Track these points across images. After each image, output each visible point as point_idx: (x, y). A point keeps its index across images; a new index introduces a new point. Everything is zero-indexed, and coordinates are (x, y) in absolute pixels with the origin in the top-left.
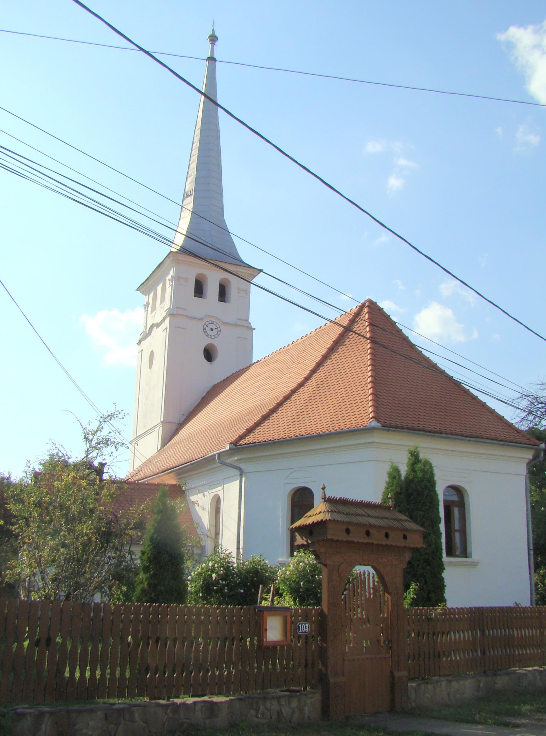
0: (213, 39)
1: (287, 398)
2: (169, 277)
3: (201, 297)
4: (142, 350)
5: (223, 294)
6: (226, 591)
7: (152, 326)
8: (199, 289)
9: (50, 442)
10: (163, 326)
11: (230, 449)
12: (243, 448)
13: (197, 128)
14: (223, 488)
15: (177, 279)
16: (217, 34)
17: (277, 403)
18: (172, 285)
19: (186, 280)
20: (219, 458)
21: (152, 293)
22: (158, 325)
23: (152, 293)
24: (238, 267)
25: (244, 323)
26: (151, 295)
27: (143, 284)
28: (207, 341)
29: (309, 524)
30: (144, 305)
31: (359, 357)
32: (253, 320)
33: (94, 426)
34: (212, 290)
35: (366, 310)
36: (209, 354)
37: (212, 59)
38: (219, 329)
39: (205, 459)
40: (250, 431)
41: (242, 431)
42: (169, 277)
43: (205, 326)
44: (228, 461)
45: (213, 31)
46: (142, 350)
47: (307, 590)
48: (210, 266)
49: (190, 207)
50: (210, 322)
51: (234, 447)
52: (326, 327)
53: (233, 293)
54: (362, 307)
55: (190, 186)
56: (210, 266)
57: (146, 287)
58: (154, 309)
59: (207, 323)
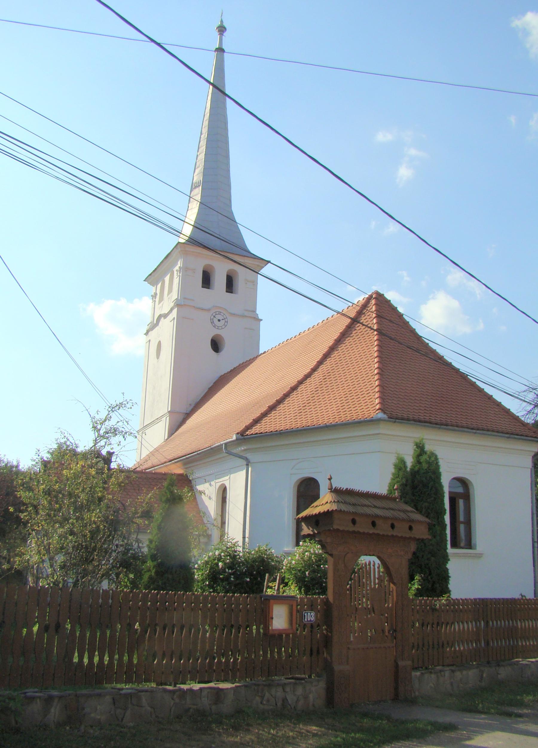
0: (222, 29)
2: (177, 268)
4: (150, 341)
6: (232, 579)
8: (207, 280)
9: (59, 431)
10: (171, 317)
11: (237, 439)
13: (205, 119)
14: (230, 478)
15: (185, 270)
16: (225, 25)
20: (226, 448)
21: (160, 284)
22: (165, 316)
23: (160, 284)
24: (246, 258)
26: (159, 286)
27: (150, 275)
28: (216, 332)
30: (152, 296)
31: (366, 349)
32: (260, 312)
33: (103, 415)
36: (216, 345)
37: (220, 50)
38: (226, 320)
39: (211, 449)
40: (256, 421)
41: (249, 421)
42: (177, 268)
45: (222, 21)
46: (150, 341)
47: (312, 579)
48: (217, 259)
49: (198, 198)
50: (218, 313)
53: (240, 284)
55: (198, 177)
56: (217, 259)
57: (154, 277)
58: (161, 299)
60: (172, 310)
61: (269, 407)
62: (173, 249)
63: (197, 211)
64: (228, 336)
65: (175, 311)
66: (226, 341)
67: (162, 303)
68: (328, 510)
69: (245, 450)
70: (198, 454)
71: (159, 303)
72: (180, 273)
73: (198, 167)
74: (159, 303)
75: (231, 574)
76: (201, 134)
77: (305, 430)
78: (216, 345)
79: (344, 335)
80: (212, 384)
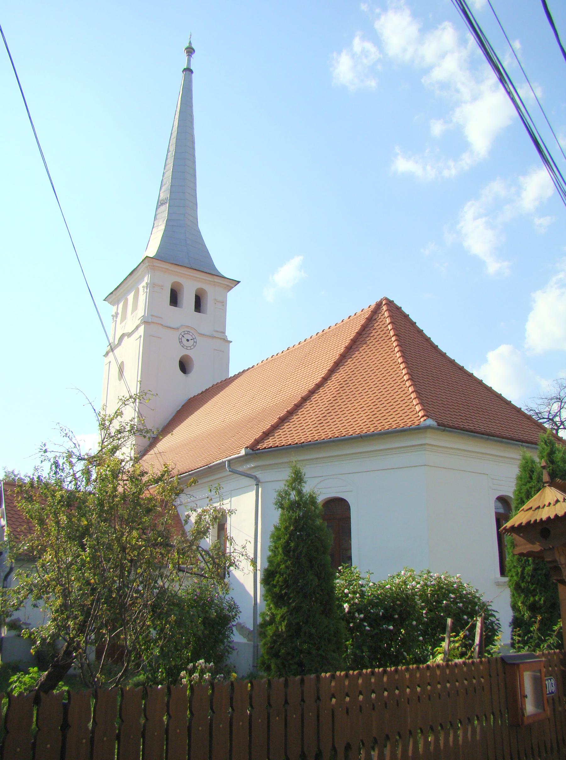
0: (190, 51)
1: (305, 399)
2: (144, 284)
3: (176, 306)
4: (110, 362)
5: (198, 305)
6: (367, 628)
7: (123, 336)
8: (174, 299)
9: (58, 427)
10: (136, 335)
11: (246, 454)
12: (263, 453)
13: (172, 137)
14: (231, 501)
15: (152, 286)
16: (194, 46)
17: (295, 405)
18: (147, 292)
19: (162, 287)
20: (229, 466)
21: (122, 303)
22: (129, 335)
23: (122, 303)
24: (215, 277)
25: (220, 335)
26: (121, 305)
27: (112, 293)
28: (184, 352)
29: (520, 525)
30: (112, 316)
31: (387, 352)
32: (229, 335)
33: (111, 411)
34: (188, 299)
35: (385, 308)
36: (184, 366)
37: (188, 71)
38: (195, 340)
39: (209, 467)
40: (267, 434)
41: (258, 434)
42: (144, 284)
43: (181, 336)
44: (240, 469)
45: (190, 43)
46: (110, 362)
47: (431, 620)
48: (185, 277)
49: (166, 214)
50: (186, 332)
51: (251, 451)
52: (294, 348)
53: (209, 303)
54: (379, 305)
55: (165, 195)
56: (185, 277)
57: (115, 296)
58: (124, 318)
59: (183, 334)
60: (137, 328)
61: (279, 418)
62: (140, 264)
63: (164, 228)
64: (196, 356)
65: (142, 328)
66: (195, 362)
67: (135, 313)
68: (549, 518)
69: (253, 468)
70: (189, 475)
71: (121, 322)
72: (147, 289)
73: (165, 185)
74: (121, 322)
75: (362, 620)
76: (168, 152)
77: (333, 441)
78: (184, 366)
79: (355, 342)
80: (180, 407)
